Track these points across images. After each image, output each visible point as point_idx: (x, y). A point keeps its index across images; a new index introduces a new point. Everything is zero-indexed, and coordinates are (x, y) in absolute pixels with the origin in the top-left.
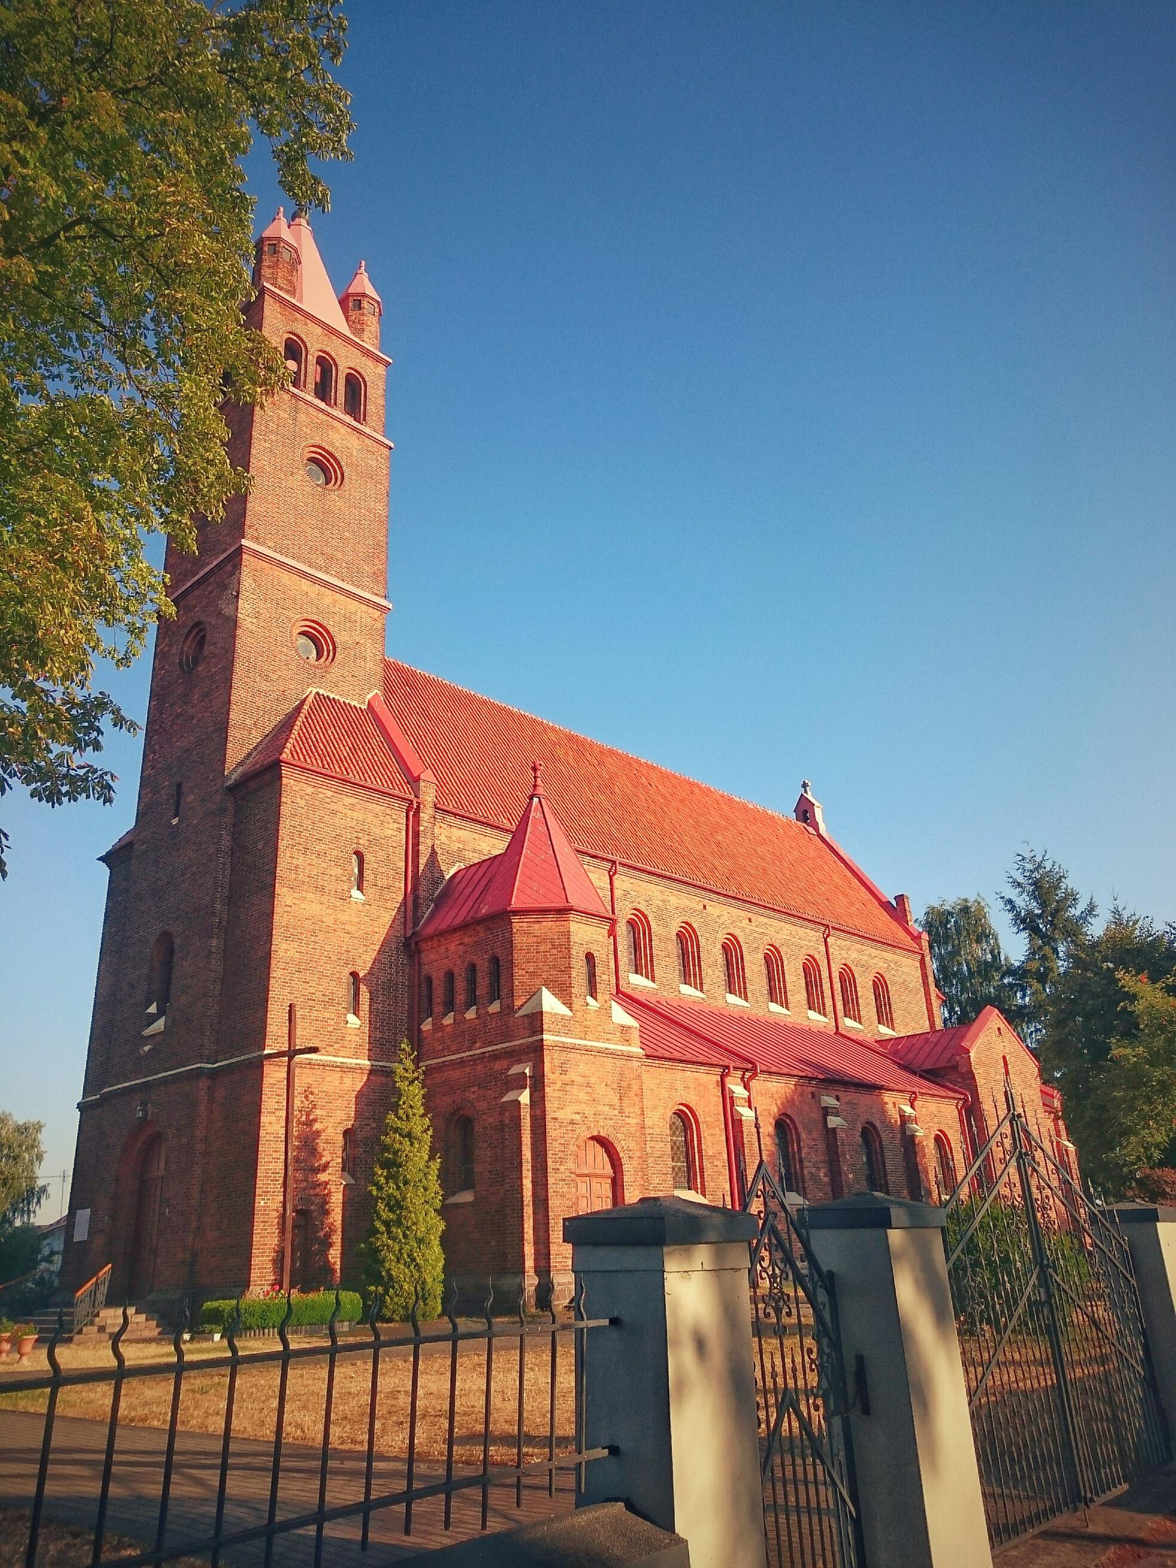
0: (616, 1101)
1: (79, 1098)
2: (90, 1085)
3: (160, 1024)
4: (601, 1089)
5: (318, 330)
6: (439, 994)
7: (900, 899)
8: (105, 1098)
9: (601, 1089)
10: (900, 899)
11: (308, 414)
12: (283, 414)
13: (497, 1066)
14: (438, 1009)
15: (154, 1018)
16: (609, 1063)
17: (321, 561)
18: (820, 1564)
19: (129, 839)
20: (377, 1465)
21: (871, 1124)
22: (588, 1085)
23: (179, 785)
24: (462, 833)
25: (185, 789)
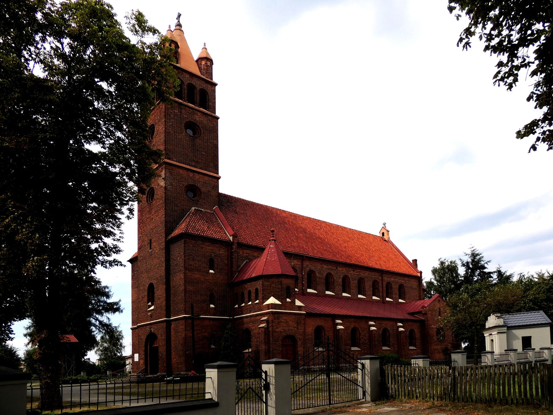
0: (296, 326)
1: (130, 326)
2: (134, 323)
3: (152, 308)
4: (291, 323)
5: (187, 76)
6: (246, 296)
7: (415, 261)
8: (138, 327)
9: (291, 323)
10: (415, 261)
11: (185, 109)
12: (176, 111)
13: (258, 318)
14: (246, 300)
15: (150, 306)
16: (293, 317)
17: (193, 164)
18: (246, 413)
19: (136, 255)
20: (105, 391)
21: (386, 329)
22: (287, 322)
23: (151, 240)
24: (247, 251)
25: (152, 241)
